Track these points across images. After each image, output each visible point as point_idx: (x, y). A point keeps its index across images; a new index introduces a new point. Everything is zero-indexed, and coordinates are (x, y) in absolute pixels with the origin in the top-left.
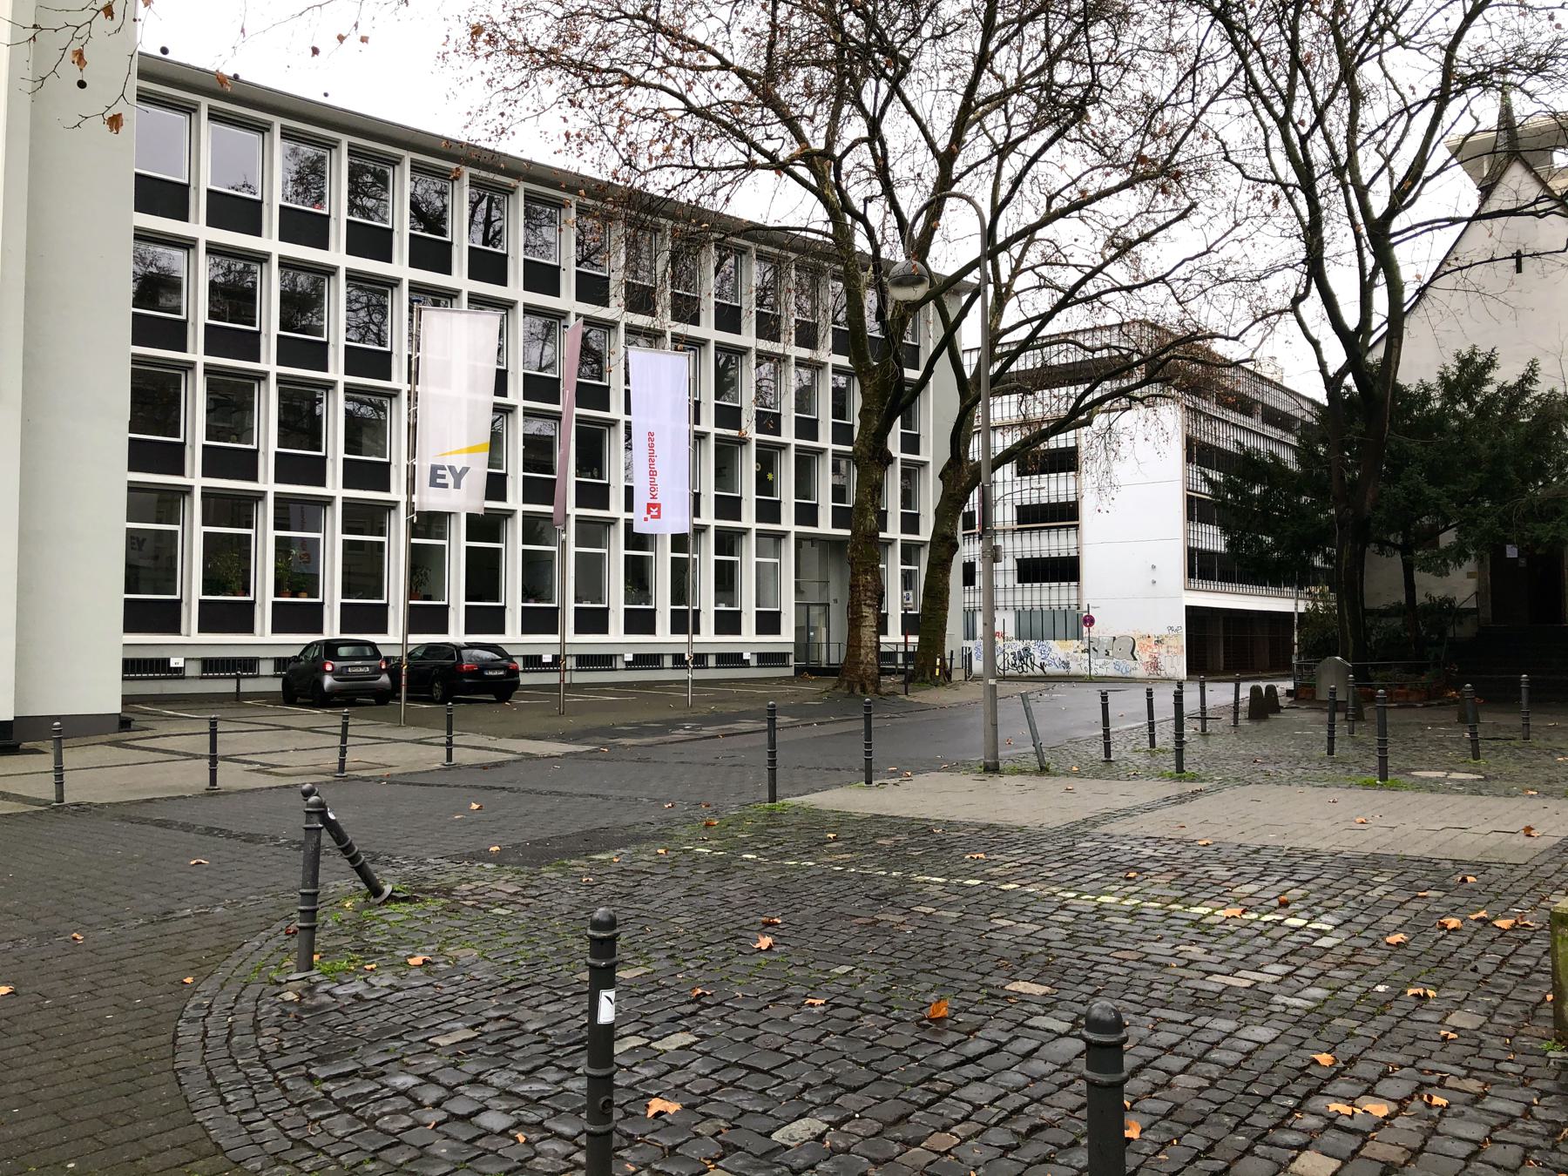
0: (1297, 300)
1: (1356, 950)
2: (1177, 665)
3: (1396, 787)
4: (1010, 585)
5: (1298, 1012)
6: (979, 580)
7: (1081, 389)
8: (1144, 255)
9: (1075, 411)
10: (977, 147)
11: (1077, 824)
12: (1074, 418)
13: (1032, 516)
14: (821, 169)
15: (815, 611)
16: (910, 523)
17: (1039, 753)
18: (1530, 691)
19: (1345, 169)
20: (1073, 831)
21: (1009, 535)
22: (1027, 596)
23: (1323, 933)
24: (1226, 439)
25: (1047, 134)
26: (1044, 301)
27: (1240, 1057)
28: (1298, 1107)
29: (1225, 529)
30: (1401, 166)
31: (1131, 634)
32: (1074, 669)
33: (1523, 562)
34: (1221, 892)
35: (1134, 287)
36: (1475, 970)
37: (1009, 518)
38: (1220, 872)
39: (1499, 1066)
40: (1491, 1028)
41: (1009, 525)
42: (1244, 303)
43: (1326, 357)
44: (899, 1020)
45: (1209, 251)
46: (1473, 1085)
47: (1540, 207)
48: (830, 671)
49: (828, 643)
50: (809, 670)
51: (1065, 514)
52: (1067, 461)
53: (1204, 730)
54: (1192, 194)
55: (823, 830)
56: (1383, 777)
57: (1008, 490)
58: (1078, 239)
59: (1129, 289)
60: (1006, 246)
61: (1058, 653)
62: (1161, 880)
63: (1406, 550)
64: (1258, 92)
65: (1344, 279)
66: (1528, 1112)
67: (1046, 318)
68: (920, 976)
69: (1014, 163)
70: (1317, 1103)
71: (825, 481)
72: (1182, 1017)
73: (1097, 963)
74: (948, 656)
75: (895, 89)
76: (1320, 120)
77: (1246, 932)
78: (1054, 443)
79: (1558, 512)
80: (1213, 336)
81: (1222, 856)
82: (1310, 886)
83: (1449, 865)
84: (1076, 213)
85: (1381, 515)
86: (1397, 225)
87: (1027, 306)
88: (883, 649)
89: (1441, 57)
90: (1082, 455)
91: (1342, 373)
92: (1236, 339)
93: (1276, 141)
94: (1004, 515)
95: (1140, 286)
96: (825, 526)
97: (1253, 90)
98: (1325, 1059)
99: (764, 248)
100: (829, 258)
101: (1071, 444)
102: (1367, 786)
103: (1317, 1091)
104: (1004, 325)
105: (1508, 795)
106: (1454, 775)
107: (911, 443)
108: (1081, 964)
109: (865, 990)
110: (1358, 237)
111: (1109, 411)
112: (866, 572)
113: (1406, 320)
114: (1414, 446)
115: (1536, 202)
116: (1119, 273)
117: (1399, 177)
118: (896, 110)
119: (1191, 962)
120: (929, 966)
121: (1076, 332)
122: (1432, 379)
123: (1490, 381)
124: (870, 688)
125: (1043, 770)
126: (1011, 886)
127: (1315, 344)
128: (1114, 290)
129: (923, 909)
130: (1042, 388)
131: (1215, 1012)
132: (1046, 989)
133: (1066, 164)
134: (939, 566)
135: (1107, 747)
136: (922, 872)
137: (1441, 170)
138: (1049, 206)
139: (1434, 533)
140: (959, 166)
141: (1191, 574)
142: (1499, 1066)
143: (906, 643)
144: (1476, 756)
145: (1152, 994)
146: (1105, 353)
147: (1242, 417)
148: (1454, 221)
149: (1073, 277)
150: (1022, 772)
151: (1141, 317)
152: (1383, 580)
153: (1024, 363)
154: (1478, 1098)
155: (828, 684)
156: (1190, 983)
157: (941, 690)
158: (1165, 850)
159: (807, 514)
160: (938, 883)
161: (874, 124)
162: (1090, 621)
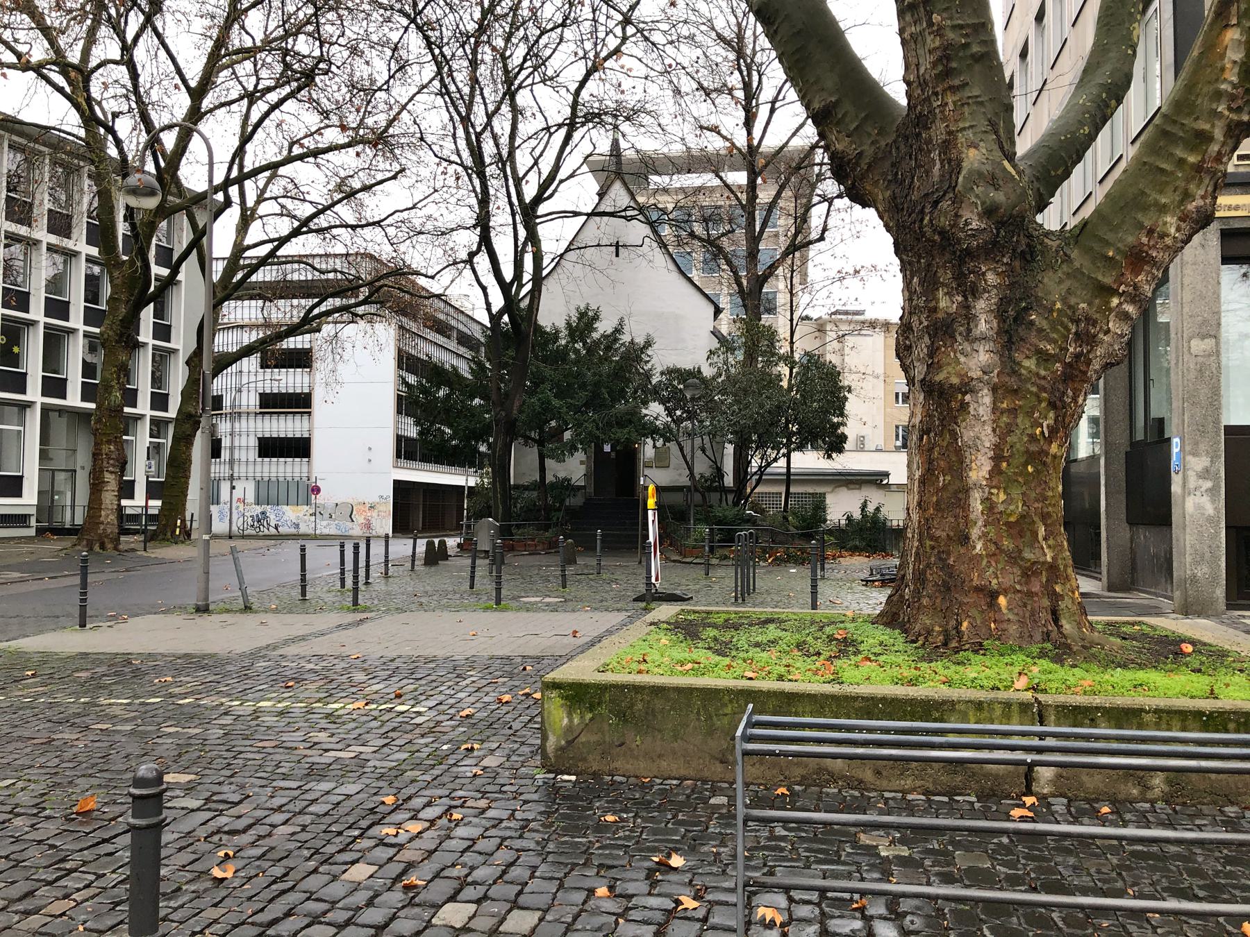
0: (472, 255)
1: (438, 723)
2: (385, 525)
3: (506, 609)
4: (251, 459)
5: (383, 771)
6: (225, 454)
7: (311, 302)
8: (366, 202)
9: (306, 320)
10: (226, 86)
11: (260, 649)
12: (307, 324)
13: (272, 403)
14: (76, 82)
15: (61, 477)
16: (160, 401)
17: (244, 595)
18: (602, 541)
19: (506, 161)
20: (256, 655)
21: (252, 418)
22: (266, 469)
23: (419, 714)
24: (423, 350)
25: (287, 90)
26: (284, 226)
27: (331, 806)
28: (361, 836)
29: (417, 423)
30: (546, 166)
31: (351, 501)
32: (303, 529)
33: (613, 454)
34: (355, 691)
35: (358, 226)
36: (510, 728)
37: (252, 402)
38: (360, 677)
39: (504, 789)
40: (507, 764)
41: (252, 409)
42: (440, 252)
43: (491, 300)
44: (48, 818)
45: (414, 207)
46: (483, 803)
47: (629, 213)
48: (73, 531)
49: (73, 507)
50: (50, 528)
51: (300, 403)
52: (302, 360)
53: (386, 573)
54: (403, 161)
55: (26, 668)
56: (498, 602)
57: (253, 378)
58: (312, 180)
59: (354, 227)
60: (255, 172)
61: (291, 516)
62: (313, 686)
63: (540, 443)
64: (448, 93)
65: (504, 246)
66: (512, 816)
67: (283, 241)
68: (78, 781)
69: (260, 108)
70: (375, 831)
71: (75, 355)
72: (294, 784)
73: (241, 752)
74: (188, 517)
75: (148, 20)
76: (489, 123)
77: (365, 718)
78: (292, 343)
79: (630, 422)
80: (418, 273)
81: (365, 666)
82: (423, 682)
83: (519, 659)
84: (311, 159)
85: (523, 417)
86: (543, 209)
87: (269, 228)
88: (129, 511)
89: (570, 98)
90: (316, 354)
91: (501, 313)
92: (432, 277)
93: (460, 132)
94: (250, 400)
95: (362, 226)
96: (74, 399)
97: (444, 92)
98: (389, 800)
99: (15, 138)
100: (88, 154)
101: (307, 346)
102: (486, 609)
103: (378, 823)
104: (249, 240)
105: (573, 611)
106: (547, 600)
107: (163, 332)
108: (226, 754)
109: (24, 798)
110: (513, 214)
111: (336, 323)
112: (109, 442)
113: (545, 282)
114: (548, 371)
115: (625, 210)
116: (345, 212)
117: (544, 176)
118: (148, 39)
119: (316, 744)
120: (90, 772)
121: (314, 256)
122: (561, 324)
123: (595, 330)
124: (109, 546)
125: (247, 608)
126: (187, 701)
127: (484, 289)
128: (341, 226)
129: (100, 726)
130: (281, 298)
131: (322, 777)
132: (193, 777)
133: (298, 118)
134: (184, 440)
135: (304, 588)
136: (110, 695)
137: (572, 176)
138: (290, 151)
139: (559, 432)
140: (206, 104)
141: (398, 456)
142: (504, 789)
143: (146, 507)
144: (564, 587)
145: (279, 771)
146: (331, 276)
147: (438, 336)
148: (576, 214)
149: (308, 210)
150: (228, 611)
151: (362, 251)
152: (523, 464)
153: (264, 275)
154: (484, 811)
155: (68, 542)
156: (309, 760)
157: (181, 546)
158: (324, 664)
159: (55, 386)
160: (121, 704)
161: (127, 49)
162: (317, 490)
